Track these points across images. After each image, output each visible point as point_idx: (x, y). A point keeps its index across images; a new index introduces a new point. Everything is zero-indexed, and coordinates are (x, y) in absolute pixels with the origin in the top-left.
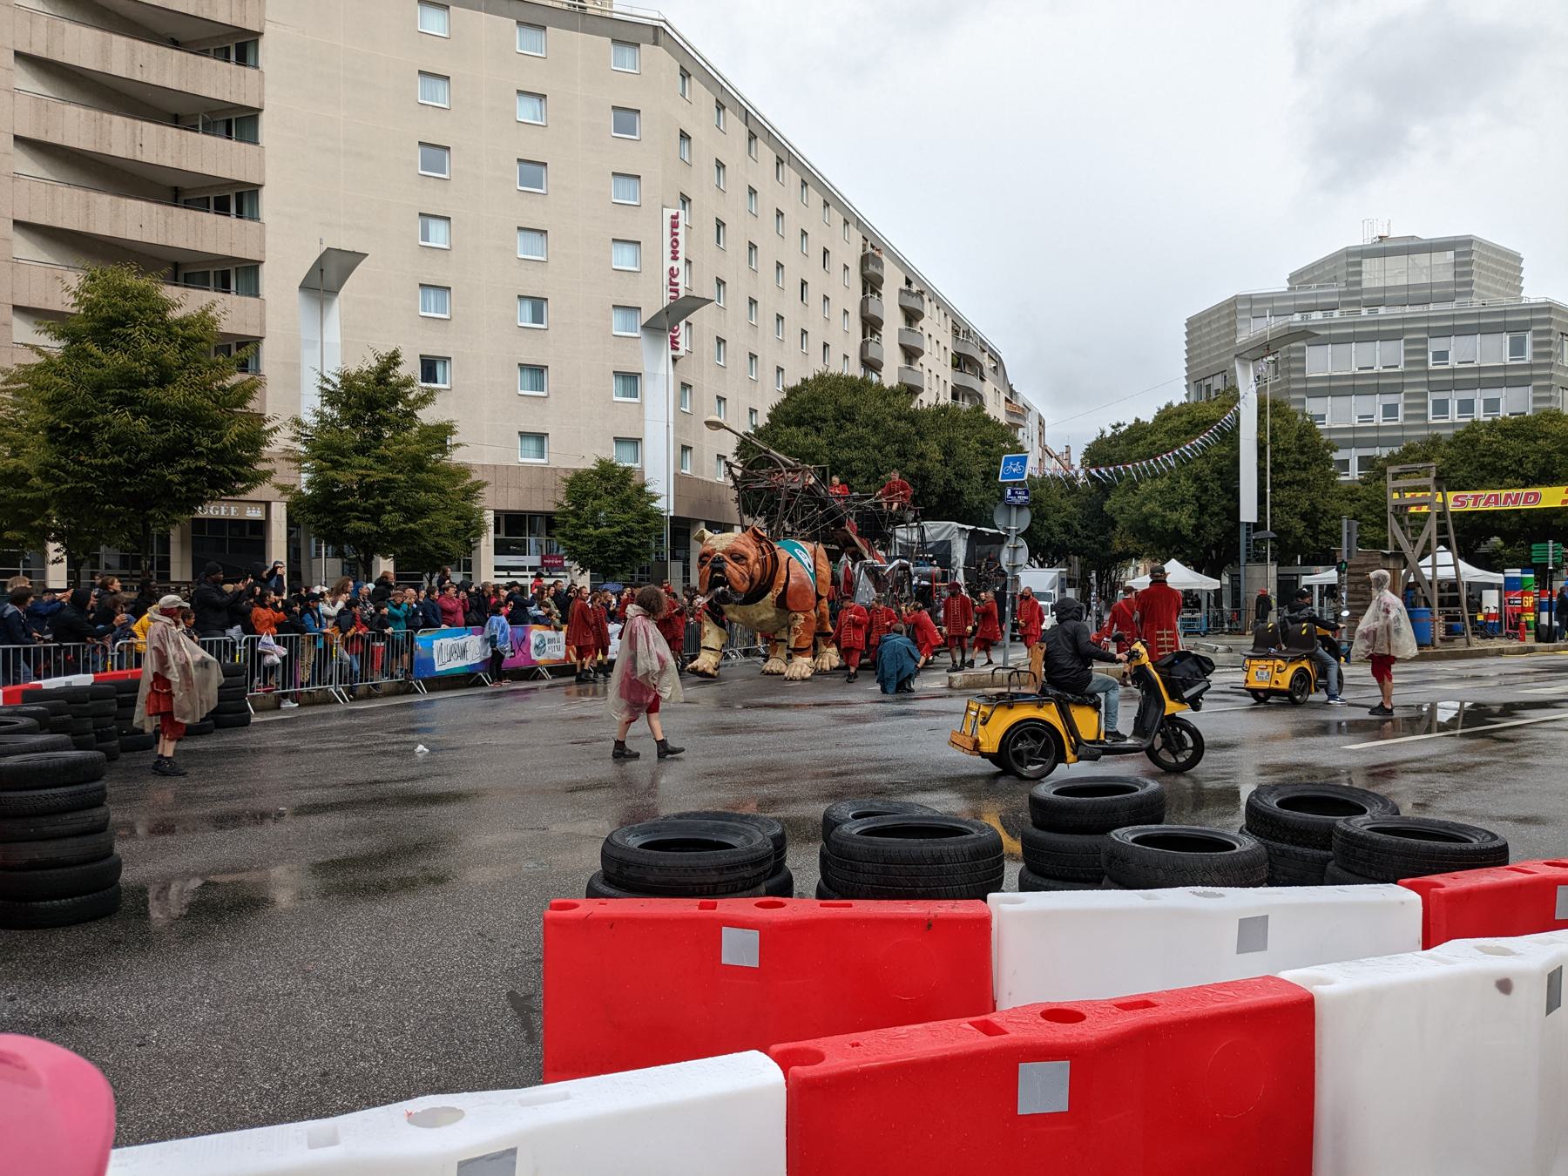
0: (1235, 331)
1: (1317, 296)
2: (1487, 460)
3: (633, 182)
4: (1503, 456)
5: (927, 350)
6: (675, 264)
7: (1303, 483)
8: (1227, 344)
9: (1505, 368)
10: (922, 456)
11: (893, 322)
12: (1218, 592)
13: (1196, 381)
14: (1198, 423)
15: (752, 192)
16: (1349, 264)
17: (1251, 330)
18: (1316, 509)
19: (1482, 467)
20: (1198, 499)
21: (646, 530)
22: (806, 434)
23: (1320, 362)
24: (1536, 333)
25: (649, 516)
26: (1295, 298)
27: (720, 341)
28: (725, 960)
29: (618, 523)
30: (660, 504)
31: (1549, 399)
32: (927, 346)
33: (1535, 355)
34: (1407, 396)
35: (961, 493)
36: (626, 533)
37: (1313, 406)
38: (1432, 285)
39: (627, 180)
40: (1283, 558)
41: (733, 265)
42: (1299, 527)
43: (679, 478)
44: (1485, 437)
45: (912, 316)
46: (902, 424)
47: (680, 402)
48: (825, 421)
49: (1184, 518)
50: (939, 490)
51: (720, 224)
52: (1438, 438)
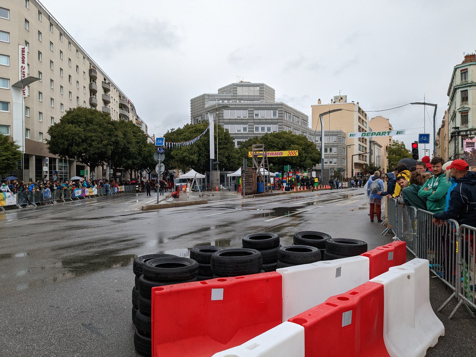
0: (204, 104)
1: (226, 96)
2: (270, 143)
3: (6, 34)
4: (273, 142)
5: (111, 101)
6: (24, 65)
7: (226, 148)
8: (202, 107)
9: (272, 119)
10: (117, 136)
11: (100, 92)
12: (204, 179)
13: (194, 117)
14: (197, 129)
15: (51, 43)
16: (234, 88)
17: (209, 104)
18: (229, 155)
19: (269, 145)
20: (199, 152)
21: (15, 159)
22: (75, 127)
23: (227, 114)
24: (279, 111)
25: (16, 154)
26: (220, 96)
27: (40, 93)
28: (222, 298)
29: (4, 156)
30: (21, 149)
31: (282, 128)
32: (111, 100)
33: (279, 116)
34: (249, 125)
35: (129, 148)
36: (7, 159)
37: (226, 127)
38: (254, 96)
39: (4, 34)
40: (221, 170)
41: (45, 68)
42: (225, 160)
43: (26, 140)
44: (270, 138)
45: (106, 90)
46: (109, 125)
47: (26, 113)
48: (82, 123)
49: (195, 157)
50: (122, 147)
51: (40, 53)
52: (257, 137)
